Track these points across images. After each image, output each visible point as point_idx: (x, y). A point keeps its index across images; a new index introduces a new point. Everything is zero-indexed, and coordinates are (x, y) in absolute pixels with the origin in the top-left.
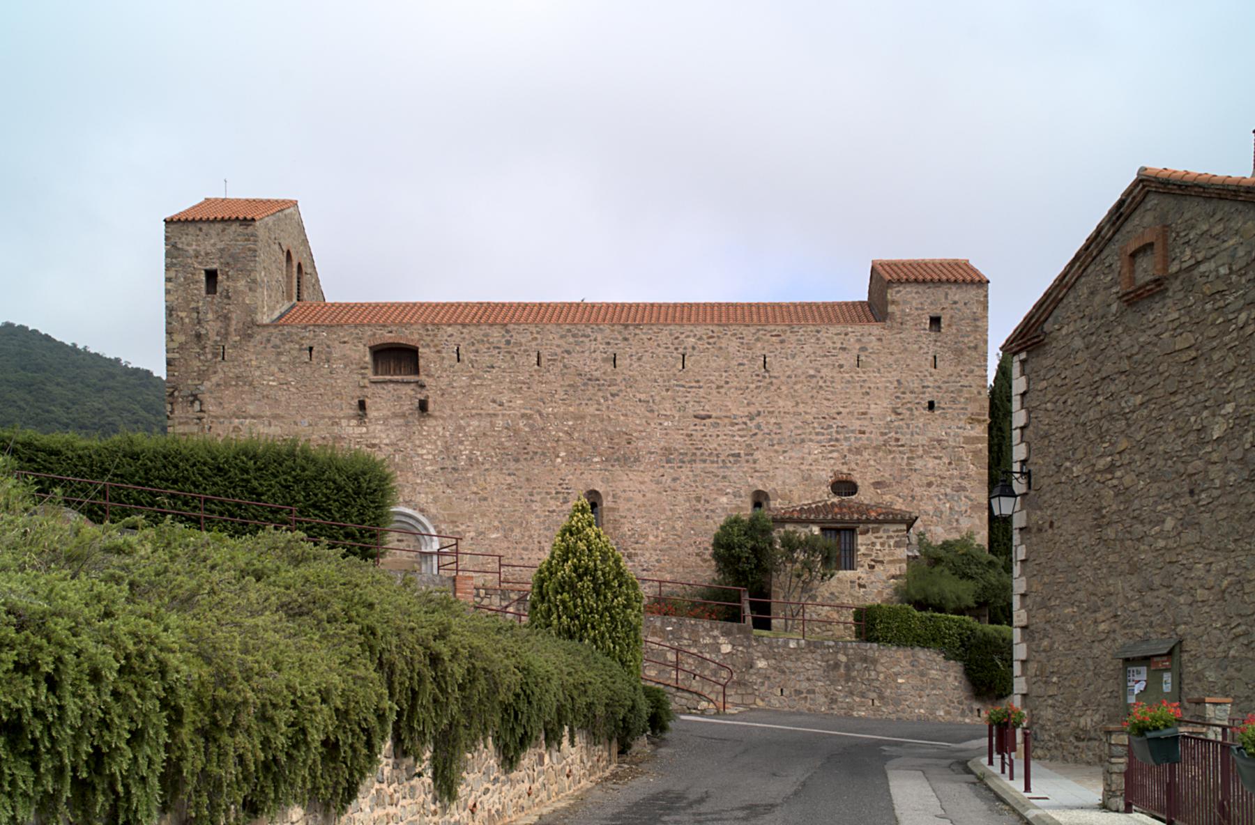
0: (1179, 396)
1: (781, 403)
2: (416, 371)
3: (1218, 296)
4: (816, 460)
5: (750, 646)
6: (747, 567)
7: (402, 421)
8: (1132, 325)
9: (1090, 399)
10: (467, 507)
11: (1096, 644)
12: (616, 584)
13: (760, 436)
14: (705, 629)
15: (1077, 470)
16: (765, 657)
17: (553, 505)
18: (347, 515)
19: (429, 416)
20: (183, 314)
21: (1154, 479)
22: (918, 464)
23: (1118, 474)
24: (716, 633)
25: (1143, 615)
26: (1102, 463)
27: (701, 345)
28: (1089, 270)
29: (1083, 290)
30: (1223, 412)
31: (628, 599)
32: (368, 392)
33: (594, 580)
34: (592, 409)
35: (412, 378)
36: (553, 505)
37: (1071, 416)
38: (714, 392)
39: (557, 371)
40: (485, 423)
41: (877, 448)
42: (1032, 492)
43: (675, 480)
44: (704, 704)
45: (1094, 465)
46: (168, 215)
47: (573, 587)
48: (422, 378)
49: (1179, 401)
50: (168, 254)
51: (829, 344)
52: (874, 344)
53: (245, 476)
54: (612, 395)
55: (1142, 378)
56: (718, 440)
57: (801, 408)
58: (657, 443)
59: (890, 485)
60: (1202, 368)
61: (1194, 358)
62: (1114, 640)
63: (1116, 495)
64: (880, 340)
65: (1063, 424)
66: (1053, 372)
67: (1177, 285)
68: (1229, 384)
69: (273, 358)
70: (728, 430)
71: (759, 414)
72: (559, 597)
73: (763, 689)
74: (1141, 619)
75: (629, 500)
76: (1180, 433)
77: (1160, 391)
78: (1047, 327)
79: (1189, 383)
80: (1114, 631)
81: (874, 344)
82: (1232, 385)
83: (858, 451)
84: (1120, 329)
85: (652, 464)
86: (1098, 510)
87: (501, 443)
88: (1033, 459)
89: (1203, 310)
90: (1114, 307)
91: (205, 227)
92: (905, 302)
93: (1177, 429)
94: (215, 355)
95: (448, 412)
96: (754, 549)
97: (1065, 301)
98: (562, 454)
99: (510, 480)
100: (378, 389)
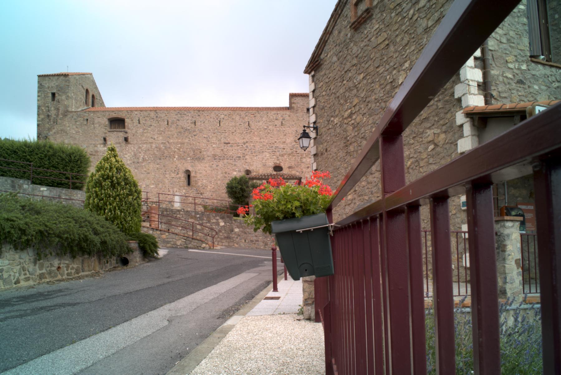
0: (381, 67)
1: (255, 138)
2: (124, 127)
3: (398, 7)
4: (268, 159)
5: (232, 223)
6: (239, 196)
7: (119, 145)
8: (357, 40)
9: (340, 84)
10: (142, 176)
11: (347, 207)
12: (123, 183)
13: (248, 150)
14: (213, 216)
15: (336, 121)
16: (238, 227)
17: (173, 175)
18: (66, 170)
19: (129, 143)
20: (43, 108)
21: (370, 115)
22: (304, 160)
23: (354, 117)
24: (218, 218)
25: (368, 188)
26: (346, 114)
27: (226, 118)
28: (338, 22)
29: (335, 32)
30: (404, 68)
31: (130, 190)
32: (107, 135)
33: (112, 182)
34: (187, 141)
35: (123, 130)
36: (173, 175)
37: (333, 95)
38: (231, 134)
39: (174, 127)
40: (149, 146)
41: (289, 154)
42: (318, 137)
43: (217, 166)
44: (204, 245)
45: (343, 116)
46: (39, 74)
47: (101, 184)
48: (126, 130)
49: (381, 69)
50: (39, 87)
51: (272, 117)
52: (287, 118)
53: (24, 154)
54: (195, 135)
55: (363, 65)
56: (233, 151)
57: (262, 140)
58: (211, 152)
59: (294, 168)
60: (392, 48)
61: (388, 45)
62: (355, 203)
63: (354, 128)
64: (289, 116)
65: (330, 99)
66: (325, 77)
67: (377, 10)
68: (406, 52)
69: (74, 123)
70: (236, 148)
71: (247, 142)
72: (94, 189)
73: (237, 240)
74: (367, 191)
75: (201, 173)
76: (382, 87)
77: (372, 68)
78: (322, 57)
79: (386, 59)
80: (355, 199)
81: (287, 118)
82: (408, 51)
83: (283, 156)
84: (352, 45)
85: (209, 160)
86: (346, 138)
87: (154, 153)
88: (318, 121)
89: (391, 17)
90: (349, 35)
91: (51, 78)
92: (298, 103)
93: (381, 85)
94: (54, 122)
95: (136, 142)
96: (241, 189)
97: (329, 41)
98: (176, 157)
99: (158, 166)
100: (111, 134)
